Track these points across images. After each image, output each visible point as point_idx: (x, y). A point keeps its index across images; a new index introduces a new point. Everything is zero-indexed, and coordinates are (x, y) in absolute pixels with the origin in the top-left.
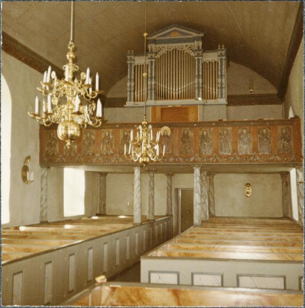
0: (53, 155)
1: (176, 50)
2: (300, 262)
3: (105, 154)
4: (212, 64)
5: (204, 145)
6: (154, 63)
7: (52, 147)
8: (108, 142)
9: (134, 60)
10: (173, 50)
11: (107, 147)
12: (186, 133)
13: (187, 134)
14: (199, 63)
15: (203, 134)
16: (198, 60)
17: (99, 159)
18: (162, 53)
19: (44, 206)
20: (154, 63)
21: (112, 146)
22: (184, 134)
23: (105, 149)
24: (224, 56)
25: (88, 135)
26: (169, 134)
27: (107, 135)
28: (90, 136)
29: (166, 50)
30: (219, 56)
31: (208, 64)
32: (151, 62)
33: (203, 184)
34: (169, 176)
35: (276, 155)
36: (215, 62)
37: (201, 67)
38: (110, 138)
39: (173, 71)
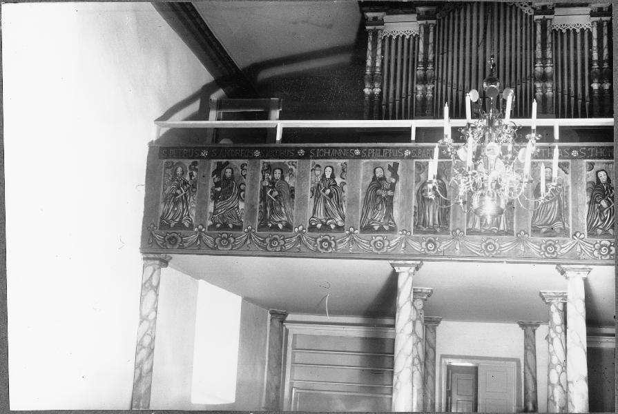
0: (180, 225)
3: (319, 226)
5: (601, 207)
6: (431, 29)
7: (176, 204)
8: (330, 195)
9: (382, 23)
11: (326, 209)
15: (598, 179)
17: (204, 237)
19: (146, 367)
20: (431, 29)
21: (339, 206)
23: (321, 215)
25: (278, 174)
27: (328, 176)
28: (282, 177)
31: (565, 36)
32: (427, 28)
36: (582, 30)
38: (336, 185)
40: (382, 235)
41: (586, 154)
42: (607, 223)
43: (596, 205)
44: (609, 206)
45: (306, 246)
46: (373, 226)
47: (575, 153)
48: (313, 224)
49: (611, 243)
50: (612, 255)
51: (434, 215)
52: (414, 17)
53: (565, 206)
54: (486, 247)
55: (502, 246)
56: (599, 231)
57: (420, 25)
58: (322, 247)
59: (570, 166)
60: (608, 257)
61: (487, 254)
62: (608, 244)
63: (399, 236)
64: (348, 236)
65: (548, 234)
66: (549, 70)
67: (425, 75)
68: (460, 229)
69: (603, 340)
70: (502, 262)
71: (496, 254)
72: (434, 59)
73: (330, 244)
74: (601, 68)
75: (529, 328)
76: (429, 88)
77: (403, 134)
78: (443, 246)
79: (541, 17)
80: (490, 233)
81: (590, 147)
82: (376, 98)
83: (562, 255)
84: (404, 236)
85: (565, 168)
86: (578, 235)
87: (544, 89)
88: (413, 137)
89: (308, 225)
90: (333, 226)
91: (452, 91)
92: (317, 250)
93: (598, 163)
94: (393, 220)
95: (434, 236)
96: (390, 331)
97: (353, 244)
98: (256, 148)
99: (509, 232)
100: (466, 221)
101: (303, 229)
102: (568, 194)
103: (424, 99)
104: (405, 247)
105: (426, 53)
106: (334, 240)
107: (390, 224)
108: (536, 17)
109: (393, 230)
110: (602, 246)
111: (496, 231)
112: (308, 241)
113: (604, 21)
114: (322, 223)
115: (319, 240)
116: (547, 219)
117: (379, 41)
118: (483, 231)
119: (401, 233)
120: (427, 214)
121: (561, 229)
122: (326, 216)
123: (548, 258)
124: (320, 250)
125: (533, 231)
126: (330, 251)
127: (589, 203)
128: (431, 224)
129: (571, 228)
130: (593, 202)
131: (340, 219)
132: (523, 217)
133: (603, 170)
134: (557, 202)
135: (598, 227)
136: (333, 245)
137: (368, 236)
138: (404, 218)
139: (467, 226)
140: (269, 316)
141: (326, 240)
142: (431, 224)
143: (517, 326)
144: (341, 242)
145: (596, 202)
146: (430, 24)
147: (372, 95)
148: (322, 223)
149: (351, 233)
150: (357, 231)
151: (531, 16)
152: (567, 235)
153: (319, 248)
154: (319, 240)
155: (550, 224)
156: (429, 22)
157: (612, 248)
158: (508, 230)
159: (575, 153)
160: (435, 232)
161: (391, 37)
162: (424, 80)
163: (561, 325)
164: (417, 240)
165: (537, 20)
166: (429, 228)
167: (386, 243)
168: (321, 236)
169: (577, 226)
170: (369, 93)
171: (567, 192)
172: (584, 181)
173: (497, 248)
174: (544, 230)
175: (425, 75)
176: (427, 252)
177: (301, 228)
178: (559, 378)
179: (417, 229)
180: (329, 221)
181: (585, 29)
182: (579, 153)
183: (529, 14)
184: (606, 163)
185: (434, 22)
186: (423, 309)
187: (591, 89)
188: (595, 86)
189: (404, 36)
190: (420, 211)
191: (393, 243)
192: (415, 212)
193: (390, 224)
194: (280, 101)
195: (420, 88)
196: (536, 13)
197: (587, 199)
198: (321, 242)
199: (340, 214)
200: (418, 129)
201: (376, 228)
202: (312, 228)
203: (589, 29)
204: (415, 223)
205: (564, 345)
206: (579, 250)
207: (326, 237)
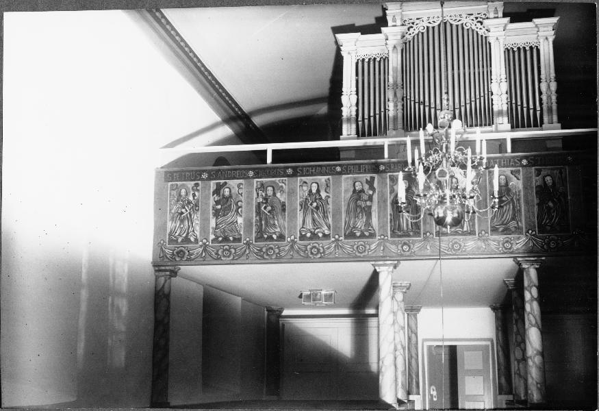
1: (445, 23)
4: (514, 52)
7: (182, 221)
8: (317, 208)
10: (439, 25)
11: (314, 220)
15: (545, 182)
18: (416, 32)
21: (325, 217)
23: (309, 225)
27: (314, 191)
28: (274, 194)
29: (426, 24)
36: (531, 48)
38: (321, 199)
42: (555, 220)
46: (355, 233)
48: (303, 233)
61: (454, 252)
78: (416, 248)
85: (517, 175)
86: (530, 232)
88: (509, 149)
90: (320, 235)
109: (372, 236)
114: (311, 232)
115: (309, 247)
116: (503, 219)
121: (515, 227)
128: (405, 228)
129: (524, 226)
133: (549, 175)
136: (355, 247)
142: (405, 228)
144: (328, 248)
150: (341, 238)
152: (521, 233)
153: (309, 254)
154: (309, 247)
164: (393, 243)
167: (368, 247)
171: (519, 195)
176: (402, 253)
177: (293, 237)
179: (393, 234)
180: (317, 231)
191: (373, 247)
192: (391, 220)
198: (311, 249)
200: (274, 152)
201: (358, 234)
204: (391, 229)
207: (315, 245)
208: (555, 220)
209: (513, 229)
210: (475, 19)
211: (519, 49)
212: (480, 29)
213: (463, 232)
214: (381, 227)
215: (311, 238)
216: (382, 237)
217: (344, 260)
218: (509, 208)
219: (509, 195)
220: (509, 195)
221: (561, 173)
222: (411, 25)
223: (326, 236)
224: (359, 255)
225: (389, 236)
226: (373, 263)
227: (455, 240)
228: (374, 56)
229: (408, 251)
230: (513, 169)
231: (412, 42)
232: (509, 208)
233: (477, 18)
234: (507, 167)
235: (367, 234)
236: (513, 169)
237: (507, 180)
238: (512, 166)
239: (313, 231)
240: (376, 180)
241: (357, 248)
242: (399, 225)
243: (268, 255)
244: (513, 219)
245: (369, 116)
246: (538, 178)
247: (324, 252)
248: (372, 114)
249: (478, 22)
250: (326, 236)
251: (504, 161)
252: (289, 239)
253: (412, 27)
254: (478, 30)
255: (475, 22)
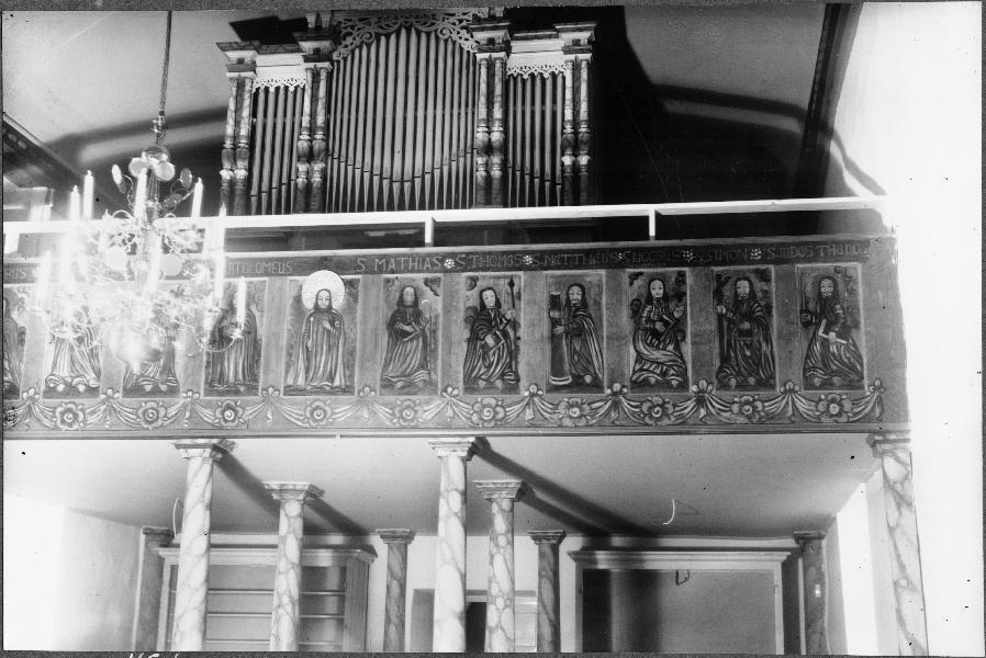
2: (384, 649)
5: (485, 346)
6: (323, 75)
12: (409, 299)
13: (416, 302)
14: (491, 76)
16: (490, 65)
20: (323, 75)
22: (401, 300)
24: (582, 51)
26: (339, 302)
30: (567, 50)
32: (316, 75)
33: (497, 546)
34: (397, 542)
35: (792, 391)
36: (554, 76)
37: (498, 90)
39: (523, 104)
40: (662, 394)
41: (464, 263)
42: (494, 371)
43: (479, 343)
44: (497, 343)
45: (39, 420)
46: (142, 386)
47: (449, 263)
48: (52, 385)
49: (498, 401)
50: (499, 420)
51: (236, 367)
52: (297, 58)
53: (433, 346)
54: (312, 414)
55: (337, 411)
56: (482, 384)
57: (307, 69)
58: (63, 422)
59: (442, 283)
60: (493, 423)
61: (313, 424)
62: (493, 402)
63: (181, 400)
64: (103, 402)
65: (407, 389)
66: (496, 136)
67: (311, 148)
68: (369, 386)
69: (647, 557)
70: (334, 436)
71: (327, 424)
72: (327, 122)
73: (76, 416)
74: (576, 132)
75: (544, 541)
76: (316, 168)
77: (413, 236)
78: (248, 413)
79: (486, 55)
80: (320, 390)
81: (472, 253)
82: (239, 187)
83: (426, 422)
84: (189, 399)
85: (435, 287)
86: (450, 390)
87: (487, 165)
88: (652, 232)
89: (43, 387)
90: (82, 388)
91: (354, 172)
92: (56, 428)
93: (484, 277)
94: (174, 375)
95: (235, 398)
96: (321, 555)
97: (110, 415)
98: (756, 246)
99: (347, 390)
100: (283, 374)
101: (35, 394)
102: (437, 329)
103: (309, 186)
104: (190, 417)
105: (313, 115)
106: (82, 410)
107: (169, 381)
108: (480, 56)
109: (173, 391)
110: (484, 406)
111: (328, 388)
112: (42, 412)
113: (581, 61)
114: (66, 383)
115: (59, 410)
116: (404, 366)
117: (247, 96)
118: (309, 388)
119: (184, 395)
120: (226, 364)
121: (425, 381)
122: (72, 371)
123: (404, 428)
124: (61, 426)
125: (383, 386)
126: (75, 427)
127: (469, 340)
128: (231, 379)
129: (439, 380)
130: (474, 339)
131: (94, 376)
132: (368, 364)
133: (490, 289)
134: (421, 339)
135: (480, 378)
136: (81, 416)
137: (134, 401)
138: (190, 372)
139: (286, 379)
140: (143, 537)
141: (69, 410)
142: (231, 379)
143: (529, 538)
144: (93, 413)
145: (478, 338)
146: (496, 59)
147: (232, 183)
148: (66, 383)
149: (109, 397)
150: (117, 395)
151: (474, 54)
152: (434, 392)
153: (59, 422)
154: (59, 410)
155: (409, 375)
156: (319, 65)
157: (498, 409)
158: (347, 386)
159: (449, 263)
160: (237, 393)
161: (267, 89)
162: (310, 156)
163: (505, 534)
164: (208, 405)
165: (481, 60)
166: (229, 386)
167: (162, 412)
168: (61, 404)
169: (449, 377)
170: (228, 178)
171: (436, 323)
172: (462, 307)
173: (328, 415)
174: (399, 384)
175: (311, 148)
176: (223, 423)
177: (32, 392)
178: (500, 617)
179: (211, 388)
180: (76, 380)
181: (536, 74)
182: (456, 263)
183: (472, 51)
184: (494, 277)
185: (326, 64)
186: (300, 516)
187: (563, 164)
188: (568, 160)
189: (286, 88)
190: (215, 361)
191: (172, 411)
192: (208, 362)
193: (169, 381)
194: (49, 192)
195: (303, 167)
196: (481, 51)
197: (466, 334)
198: (62, 414)
199: (93, 369)
200: (658, 216)
201: (148, 388)
202: (50, 392)
203: (541, 74)
204: (206, 379)
205: (509, 564)
206: (450, 413)
207: (70, 406)
208: (494, 371)
209: (421, 385)
210: (457, 23)
211: (532, 75)
212: (466, 40)
213: (332, 388)
214: (189, 376)
215: (65, 394)
216: (190, 394)
217: (273, 433)
218: (417, 346)
219: (418, 323)
220: (418, 323)
221: (511, 284)
222: (349, 30)
223: (92, 391)
224: (146, 426)
225: (202, 392)
226: (175, 441)
227: (317, 403)
228: (266, 84)
229: (233, 421)
230: (430, 276)
231: (349, 58)
232: (417, 346)
233: (461, 21)
234: (419, 271)
235: (163, 388)
236: (430, 276)
237: (416, 295)
238: (428, 271)
239: (69, 380)
240: (689, 280)
241: (144, 414)
242: (222, 374)
243: (651, 417)
244: (423, 365)
245: (280, 184)
246: (469, 293)
247: (85, 420)
248: (284, 180)
249: (463, 28)
250: (92, 391)
251: (414, 261)
252: (25, 395)
253: (351, 34)
254: (462, 41)
255: (457, 28)
